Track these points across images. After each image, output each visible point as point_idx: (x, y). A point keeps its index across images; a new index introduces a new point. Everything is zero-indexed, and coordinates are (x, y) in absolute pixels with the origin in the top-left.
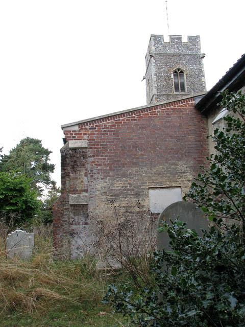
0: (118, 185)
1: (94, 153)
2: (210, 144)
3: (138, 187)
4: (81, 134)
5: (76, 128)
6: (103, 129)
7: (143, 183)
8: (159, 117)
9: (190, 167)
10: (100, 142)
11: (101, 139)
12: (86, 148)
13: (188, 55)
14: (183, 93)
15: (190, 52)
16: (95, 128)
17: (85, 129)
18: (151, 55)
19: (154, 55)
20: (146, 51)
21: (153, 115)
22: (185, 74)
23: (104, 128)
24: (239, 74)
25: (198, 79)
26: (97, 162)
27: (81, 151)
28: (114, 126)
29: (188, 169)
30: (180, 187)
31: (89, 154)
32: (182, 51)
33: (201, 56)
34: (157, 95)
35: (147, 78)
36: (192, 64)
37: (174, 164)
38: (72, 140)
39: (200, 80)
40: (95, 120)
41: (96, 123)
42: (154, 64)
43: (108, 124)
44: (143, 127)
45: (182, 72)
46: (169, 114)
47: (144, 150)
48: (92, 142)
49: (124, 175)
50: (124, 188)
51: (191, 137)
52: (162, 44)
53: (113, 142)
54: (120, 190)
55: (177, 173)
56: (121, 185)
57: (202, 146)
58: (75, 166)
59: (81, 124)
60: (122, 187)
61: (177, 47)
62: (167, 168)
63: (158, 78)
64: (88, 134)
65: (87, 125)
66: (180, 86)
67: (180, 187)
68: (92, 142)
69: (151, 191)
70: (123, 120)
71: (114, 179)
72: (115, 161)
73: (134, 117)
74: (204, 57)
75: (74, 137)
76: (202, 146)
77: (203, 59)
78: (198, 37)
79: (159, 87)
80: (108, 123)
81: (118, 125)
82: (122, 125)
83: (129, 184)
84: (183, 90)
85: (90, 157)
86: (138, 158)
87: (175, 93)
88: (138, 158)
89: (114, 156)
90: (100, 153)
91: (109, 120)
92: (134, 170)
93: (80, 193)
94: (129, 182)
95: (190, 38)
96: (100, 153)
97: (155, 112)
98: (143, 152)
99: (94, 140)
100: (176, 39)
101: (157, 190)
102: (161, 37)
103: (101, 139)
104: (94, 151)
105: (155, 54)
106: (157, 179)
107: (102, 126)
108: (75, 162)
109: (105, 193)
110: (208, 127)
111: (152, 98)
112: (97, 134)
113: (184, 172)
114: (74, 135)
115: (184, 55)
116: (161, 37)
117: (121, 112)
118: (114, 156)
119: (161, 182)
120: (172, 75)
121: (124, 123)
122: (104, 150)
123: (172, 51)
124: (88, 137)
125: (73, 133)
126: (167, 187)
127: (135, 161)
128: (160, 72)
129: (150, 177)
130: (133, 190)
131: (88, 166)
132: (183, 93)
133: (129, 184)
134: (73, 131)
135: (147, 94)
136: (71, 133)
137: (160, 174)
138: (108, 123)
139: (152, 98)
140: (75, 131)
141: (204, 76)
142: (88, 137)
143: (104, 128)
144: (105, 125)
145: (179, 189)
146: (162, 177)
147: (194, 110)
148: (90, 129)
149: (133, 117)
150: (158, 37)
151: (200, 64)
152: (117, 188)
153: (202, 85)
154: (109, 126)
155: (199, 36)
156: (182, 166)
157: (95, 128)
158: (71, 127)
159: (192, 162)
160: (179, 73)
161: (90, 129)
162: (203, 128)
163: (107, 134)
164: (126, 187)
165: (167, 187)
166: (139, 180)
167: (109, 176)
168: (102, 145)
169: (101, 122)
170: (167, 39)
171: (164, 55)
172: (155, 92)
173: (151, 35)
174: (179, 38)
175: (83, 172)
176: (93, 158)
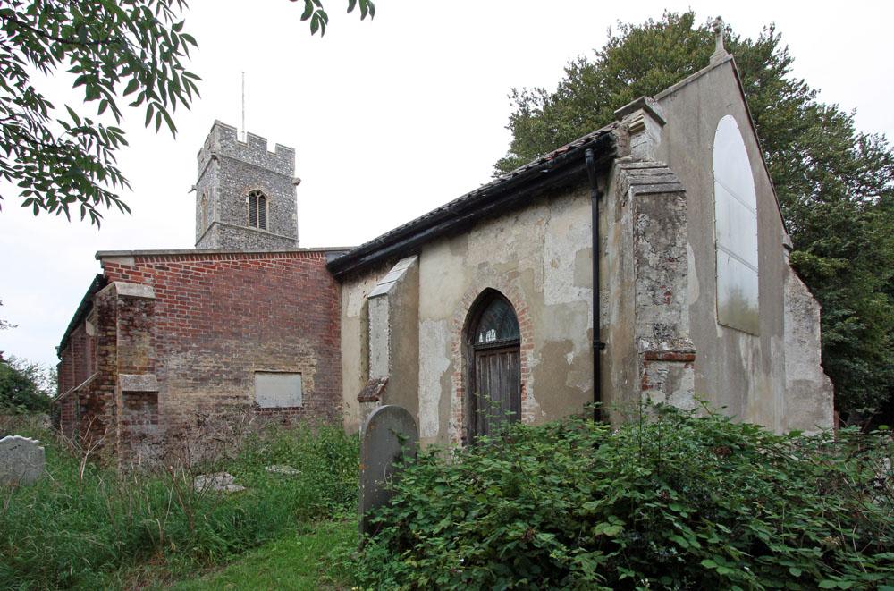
0: (207, 364)
1: (165, 310)
2: (342, 320)
3: (238, 369)
4: (140, 274)
5: (131, 262)
6: (181, 272)
7: (247, 364)
8: (274, 270)
9: (314, 348)
10: (176, 293)
11: (177, 289)
12: (153, 299)
13: (275, 173)
14: (263, 231)
15: (278, 170)
16: (168, 269)
17: (148, 266)
18: (213, 156)
19: (219, 158)
20: (200, 144)
21: (265, 265)
22: (267, 202)
23: (184, 272)
24: (403, 243)
25: (287, 215)
26: (171, 324)
27: (143, 303)
28: (203, 271)
29: (312, 350)
30: (300, 373)
31: (158, 309)
32: (264, 163)
33: (294, 181)
34: (221, 224)
35: (200, 189)
36: (281, 190)
37: (291, 341)
38: (122, 281)
39: (290, 217)
40: (151, 256)
41: (147, 261)
42: (218, 172)
43: (191, 267)
44: (250, 281)
45: (263, 197)
46: (288, 269)
47: (251, 315)
48: (161, 291)
49: (217, 349)
50: (216, 369)
51: (319, 307)
52: (234, 143)
53: (199, 296)
54: (208, 371)
55: (296, 355)
56: (212, 365)
57: (331, 321)
58: (131, 328)
59: (139, 256)
60: (214, 367)
61: (259, 156)
62: (283, 346)
63: (223, 197)
64: (154, 276)
65: (152, 261)
66: (257, 218)
67: (300, 373)
68: (161, 291)
69: (258, 377)
70: (217, 264)
71: (201, 354)
72: (203, 327)
73: (236, 263)
74: (298, 183)
75: (123, 276)
76: (331, 321)
77: (297, 187)
78: (290, 152)
79: (225, 212)
80: (192, 265)
81: (208, 272)
82: (215, 272)
83: (225, 363)
84: (264, 226)
85: (158, 314)
86: (240, 326)
87: (250, 227)
88: (240, 326)
89: (200, 318)
90: (175, 312)
91: (193, 260)
92: (233, 343)
93: (140, 373)
94: (224, 360)
95: (280, 148)
96: (175, 312)
97: (269, 261)
98: (248, 319)
99: (165, 287)
100: (257, 142)
101: (267, 376)
102: (232, 131)
103: (177, 289)
104: (164, 305)
105: (220, 155)
106: (267, 360)
107: (180, 266)
108: (131, 320)
109: (184, 375)
110: (341, 297)
111: (211, 227)
112: (171, 279)
113: (306, 354)
114: (124, 274)
115: (267, 171)
116: (233, 131)
117: (175, 251)
118: (200, 318)
119: (274, 365)
120: (248, 200)
121: (219, 269)
122: (183, 307)
123: (250, 160)
124: (154, 281)
125: (124, 269)
126: (282, 373)
127: (234, 330)
128: (226, 188)
129: (258, 356)
130: (231, 372)
131: (155, 330)
132: (263, 231)
133: (225, 363)
134: (122, 266)
135: (198, 217)
136: (120, 268)
137: (272, 353)
138: (192, 264)
139: (211, 227)
140: (128, 267)
141: (296, 213)
142: (154, 281)
143: (184, 272)
144: (185, 267)
145: (298, 376)
146: (275, 358)
147: (324, 269)
148: (157, 267)
149: (233, 263)
150: (229, 130)
151: (291, 193)
152: (203, 369)
153: (291, 225)
154: (193, 269)
155: (294, 150)
156: (303, 344)
157: (168, 269)
158: (120, 259)
159: (317, 341)
160: (258, 198)
161: (157, 267)
162: (336, 298)
163: (189, 281)
164: (220, 367)
165: (282, 373)
166: (240, 359)
167: (190, 348)
168: (180, 298)
169: (178, 261)
170: (242, 138)
171: (236, 162)
172: (216, 217)
173: (216, 121)
174: (263, 142)
175: (147, 338)
176: (161, 317)
